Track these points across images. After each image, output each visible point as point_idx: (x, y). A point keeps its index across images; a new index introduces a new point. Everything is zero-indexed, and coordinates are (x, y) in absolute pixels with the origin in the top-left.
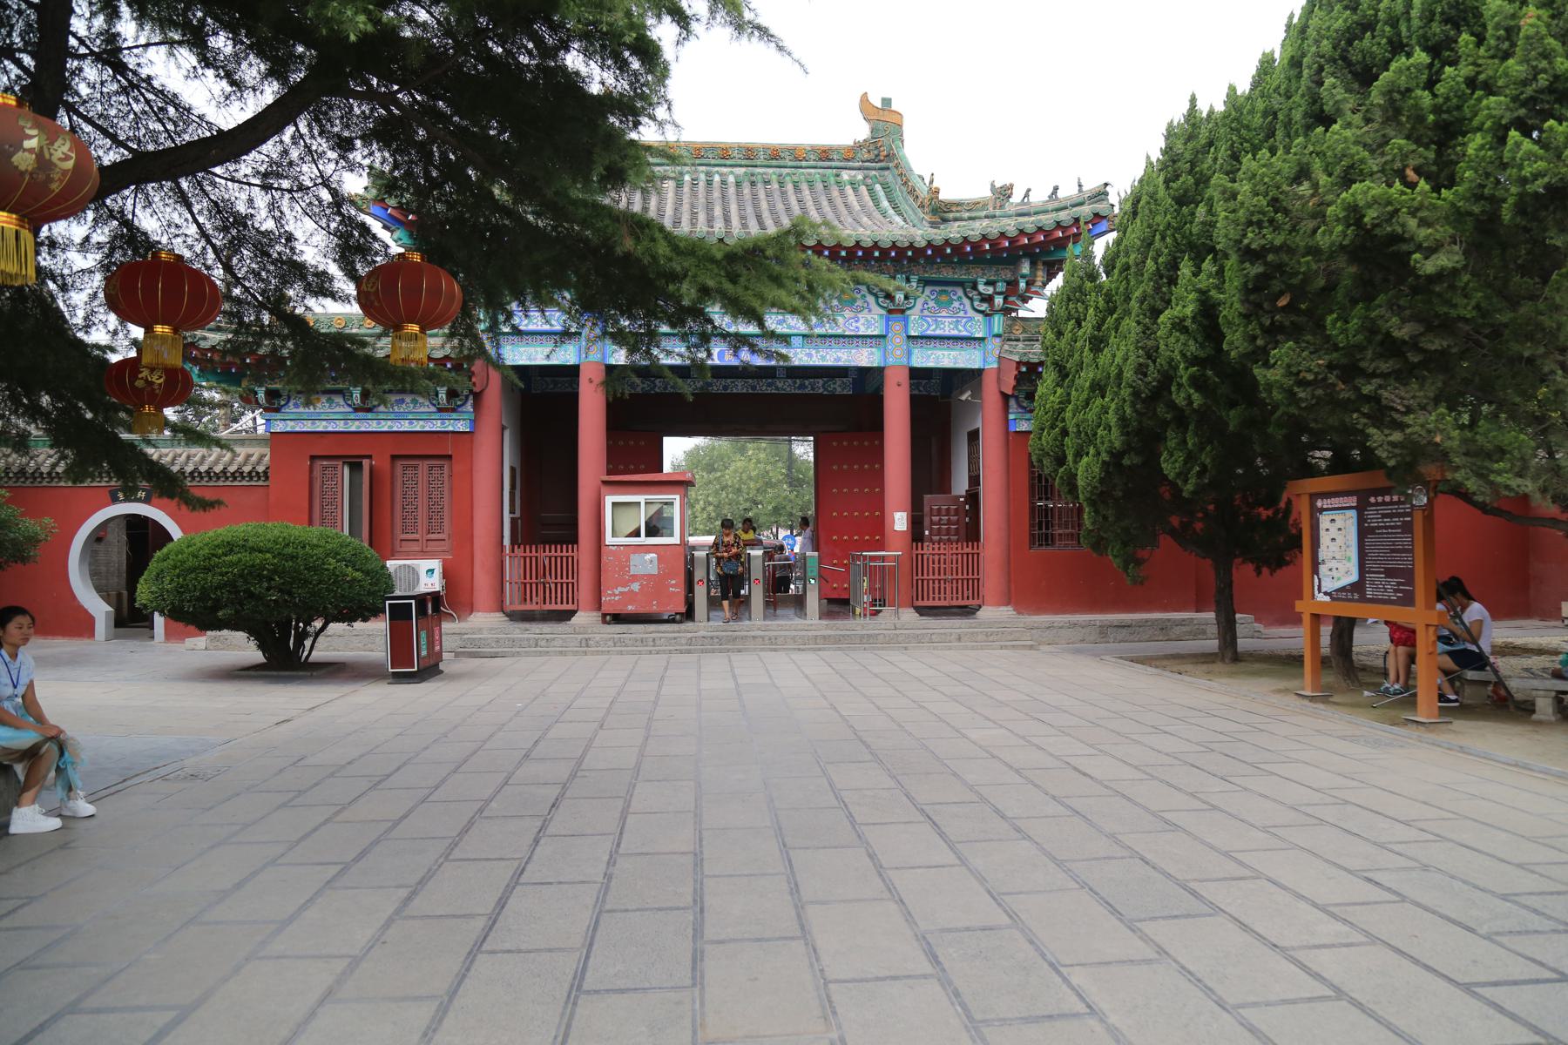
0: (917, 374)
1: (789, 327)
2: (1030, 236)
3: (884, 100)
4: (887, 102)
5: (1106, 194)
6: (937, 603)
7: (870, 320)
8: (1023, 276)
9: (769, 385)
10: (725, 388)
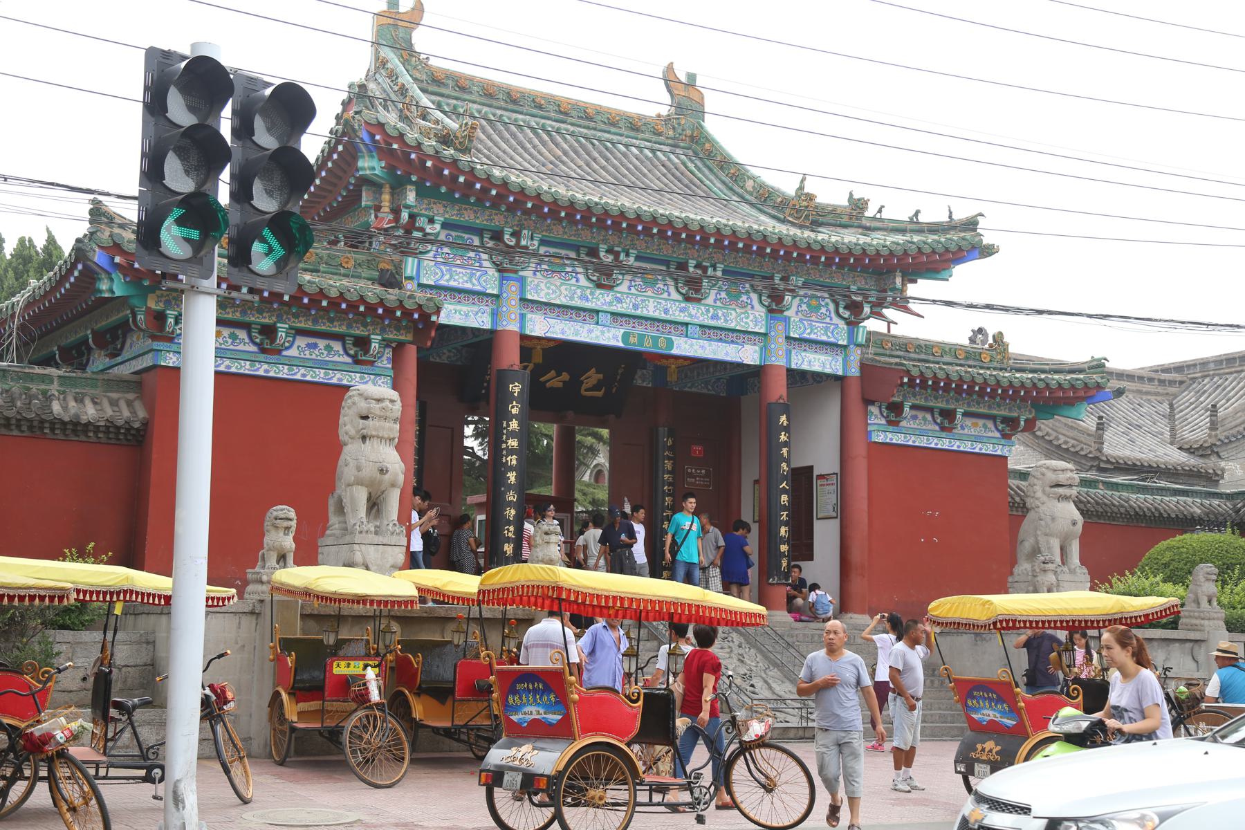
0: (528, 344)
1: (691, 316)
4: (692, 77)
7: (753, 316)
8: (408, 207)
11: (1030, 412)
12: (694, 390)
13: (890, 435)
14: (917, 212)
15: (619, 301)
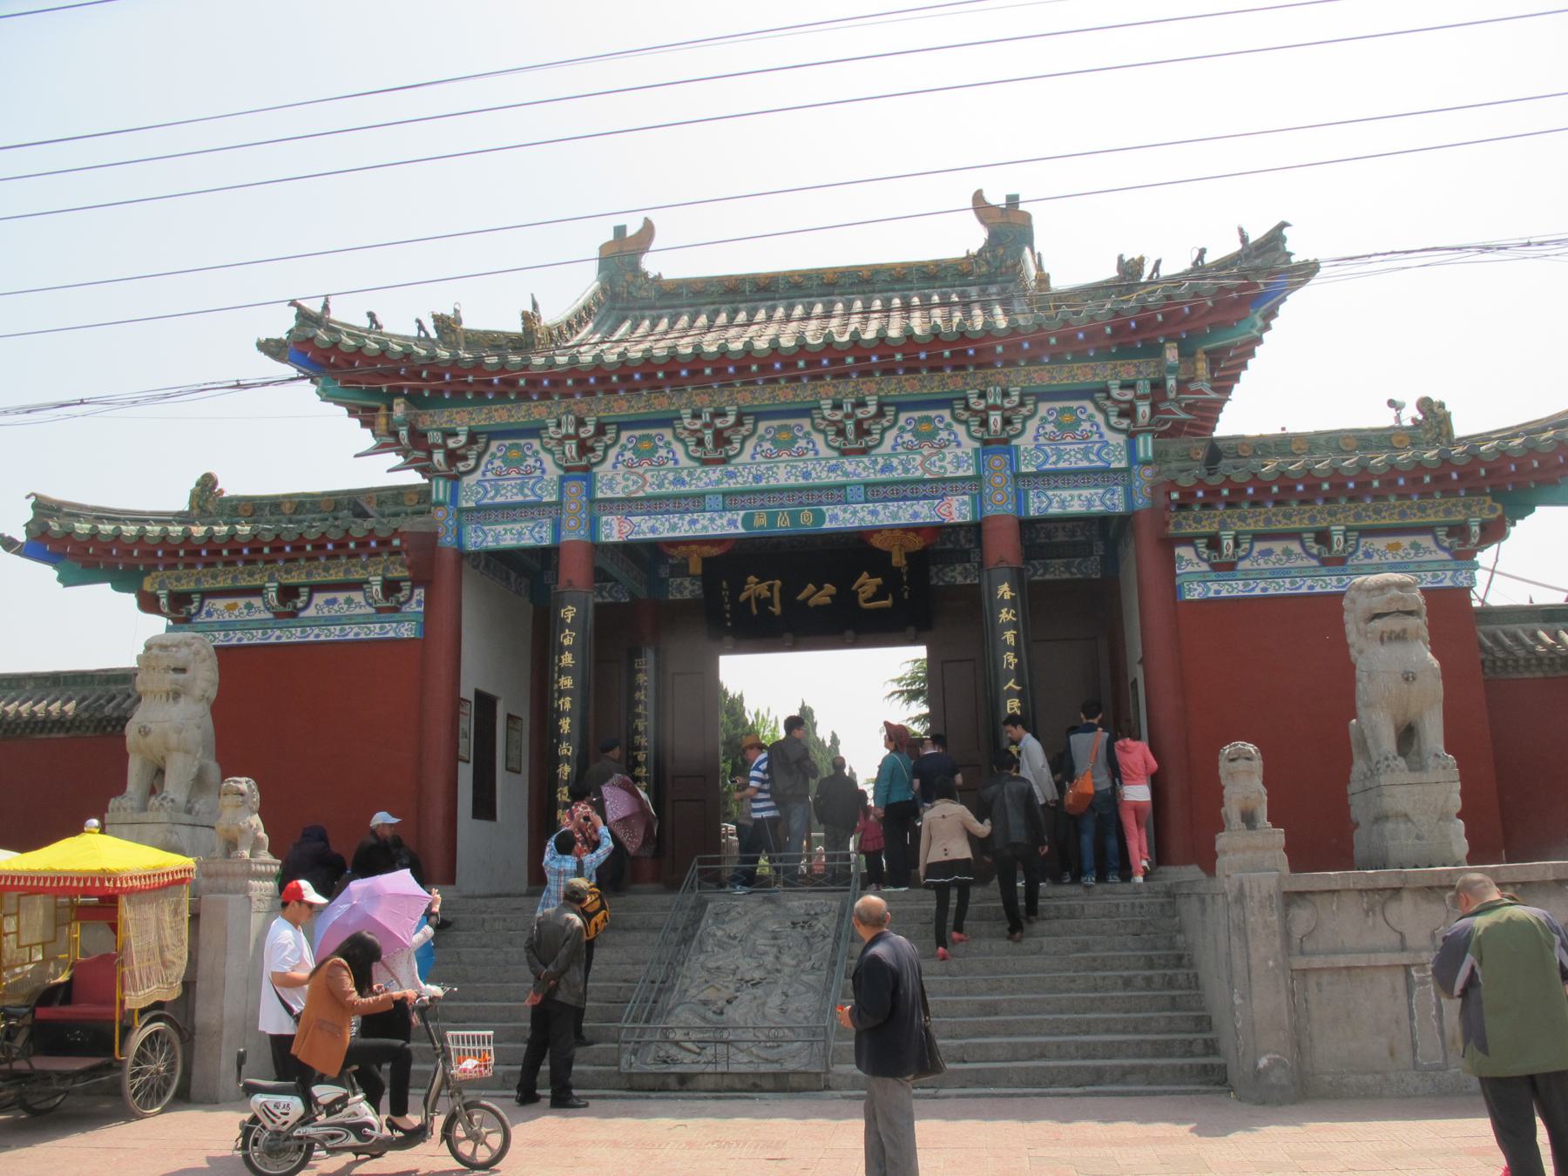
1: (846, 474)
4: (1013, 201)
8: (1172, 370)
11: (1492, 509)
12: (1048, 577)
13: (1215, 587)
14: (1202, 252)
15: (731, 475)
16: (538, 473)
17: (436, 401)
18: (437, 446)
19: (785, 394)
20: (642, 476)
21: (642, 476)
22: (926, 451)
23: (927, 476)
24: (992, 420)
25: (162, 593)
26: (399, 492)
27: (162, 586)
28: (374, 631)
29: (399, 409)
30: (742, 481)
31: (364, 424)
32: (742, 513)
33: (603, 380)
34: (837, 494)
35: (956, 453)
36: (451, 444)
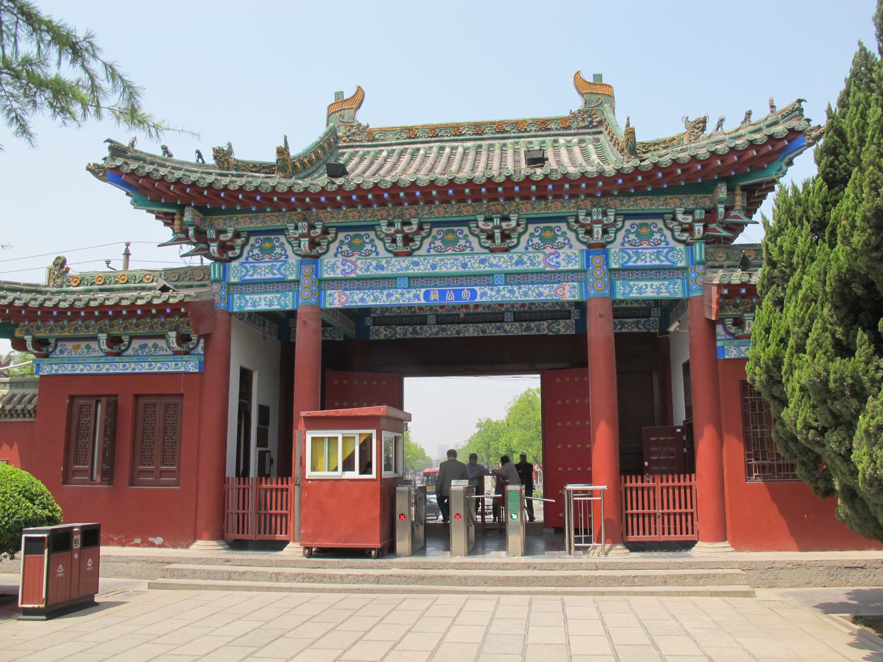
1: (491, 265)
2: (723, 158)
3: (595, 76)
5: (801, 110)
6: (647, 538)
9: (498, 328)
10: (458, 332)
15: (416, 264)
16: (283, 258)
17: (216, 211)
18: (213, 241)
19: (451, 212)
20: (354, 263)
21: (354, 263)
22: (548, 250)
23: (548, 269)
24: (595, 230)
25: (28, 339)
26: (189, 271)
27: (28, 332)
28: (171, 367)
29: (188, 217)
30: (423, 268)
31: (166, 224)
32: (423, 290)
33: (363, 198)
34: (486, 278)
35: (570, 255)
36: (222, 238)
